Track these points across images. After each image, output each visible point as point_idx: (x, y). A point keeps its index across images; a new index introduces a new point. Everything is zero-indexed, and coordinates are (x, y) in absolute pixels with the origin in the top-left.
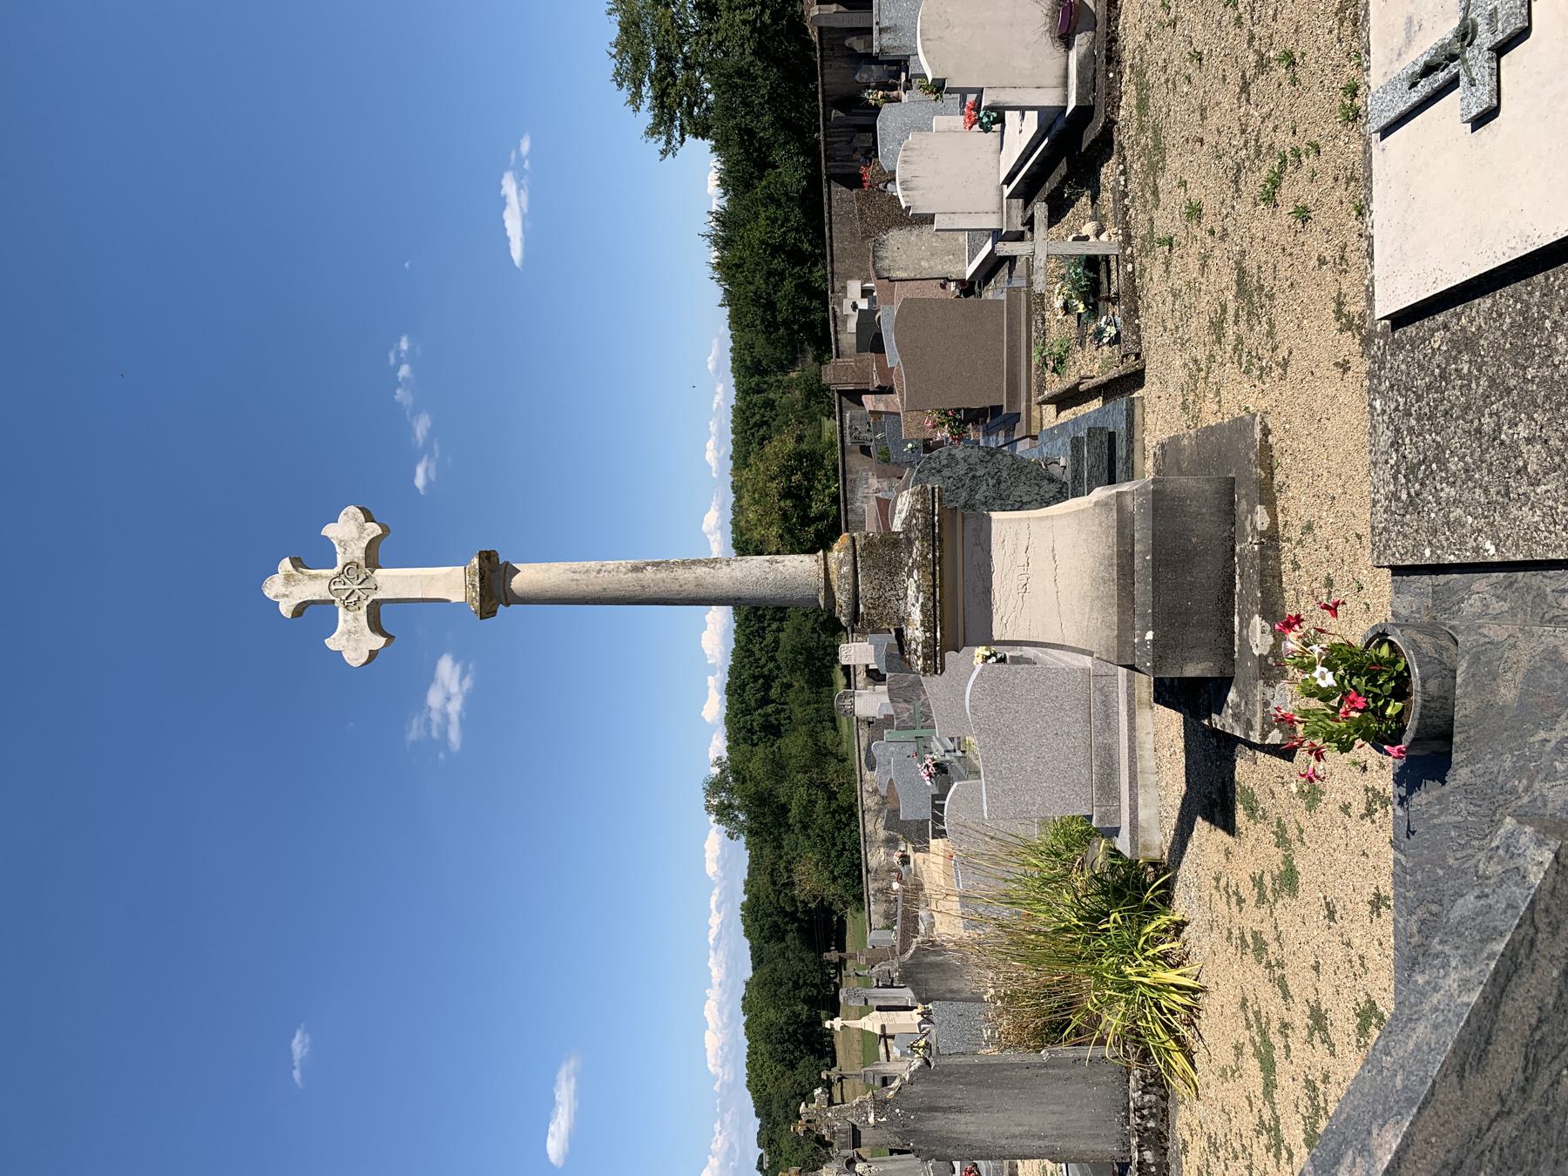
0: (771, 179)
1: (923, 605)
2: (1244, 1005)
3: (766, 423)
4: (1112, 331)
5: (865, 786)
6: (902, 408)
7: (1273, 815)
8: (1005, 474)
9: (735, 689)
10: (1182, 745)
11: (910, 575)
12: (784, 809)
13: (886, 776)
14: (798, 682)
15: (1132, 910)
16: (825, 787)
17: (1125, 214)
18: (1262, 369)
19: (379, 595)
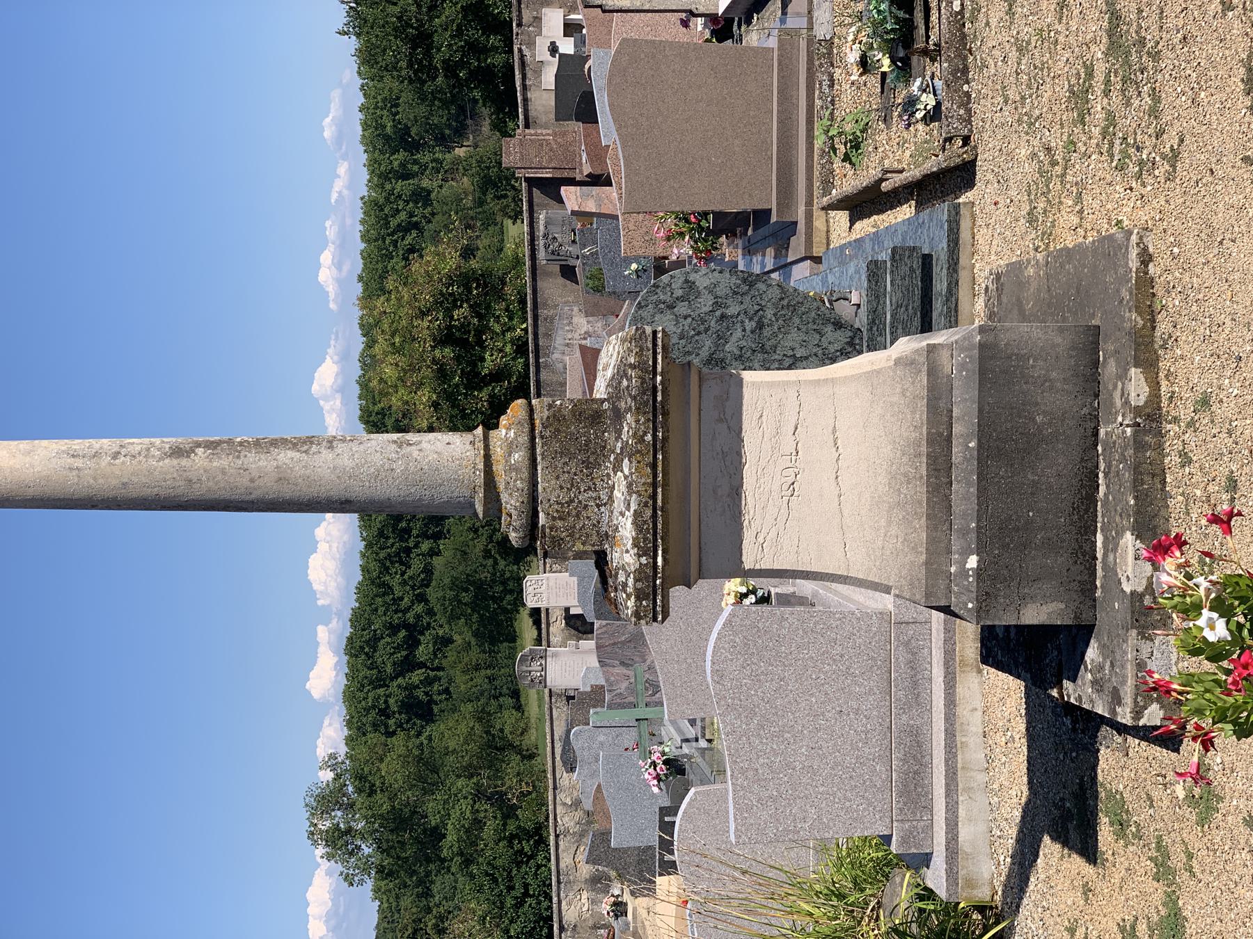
1: (637, 514)
3: (416, 226)
4: (928, 100)
5: (561, 796)
6: (628, 213)
7: (1150, 832)
8: (769, 313)
9: (361, 648)
10: (1022, 727)
11: (617, 467)
12: (437, 835)
13: (592, 782)
14: (462, 634)
16: (499, 799)
18: (1141, 163)
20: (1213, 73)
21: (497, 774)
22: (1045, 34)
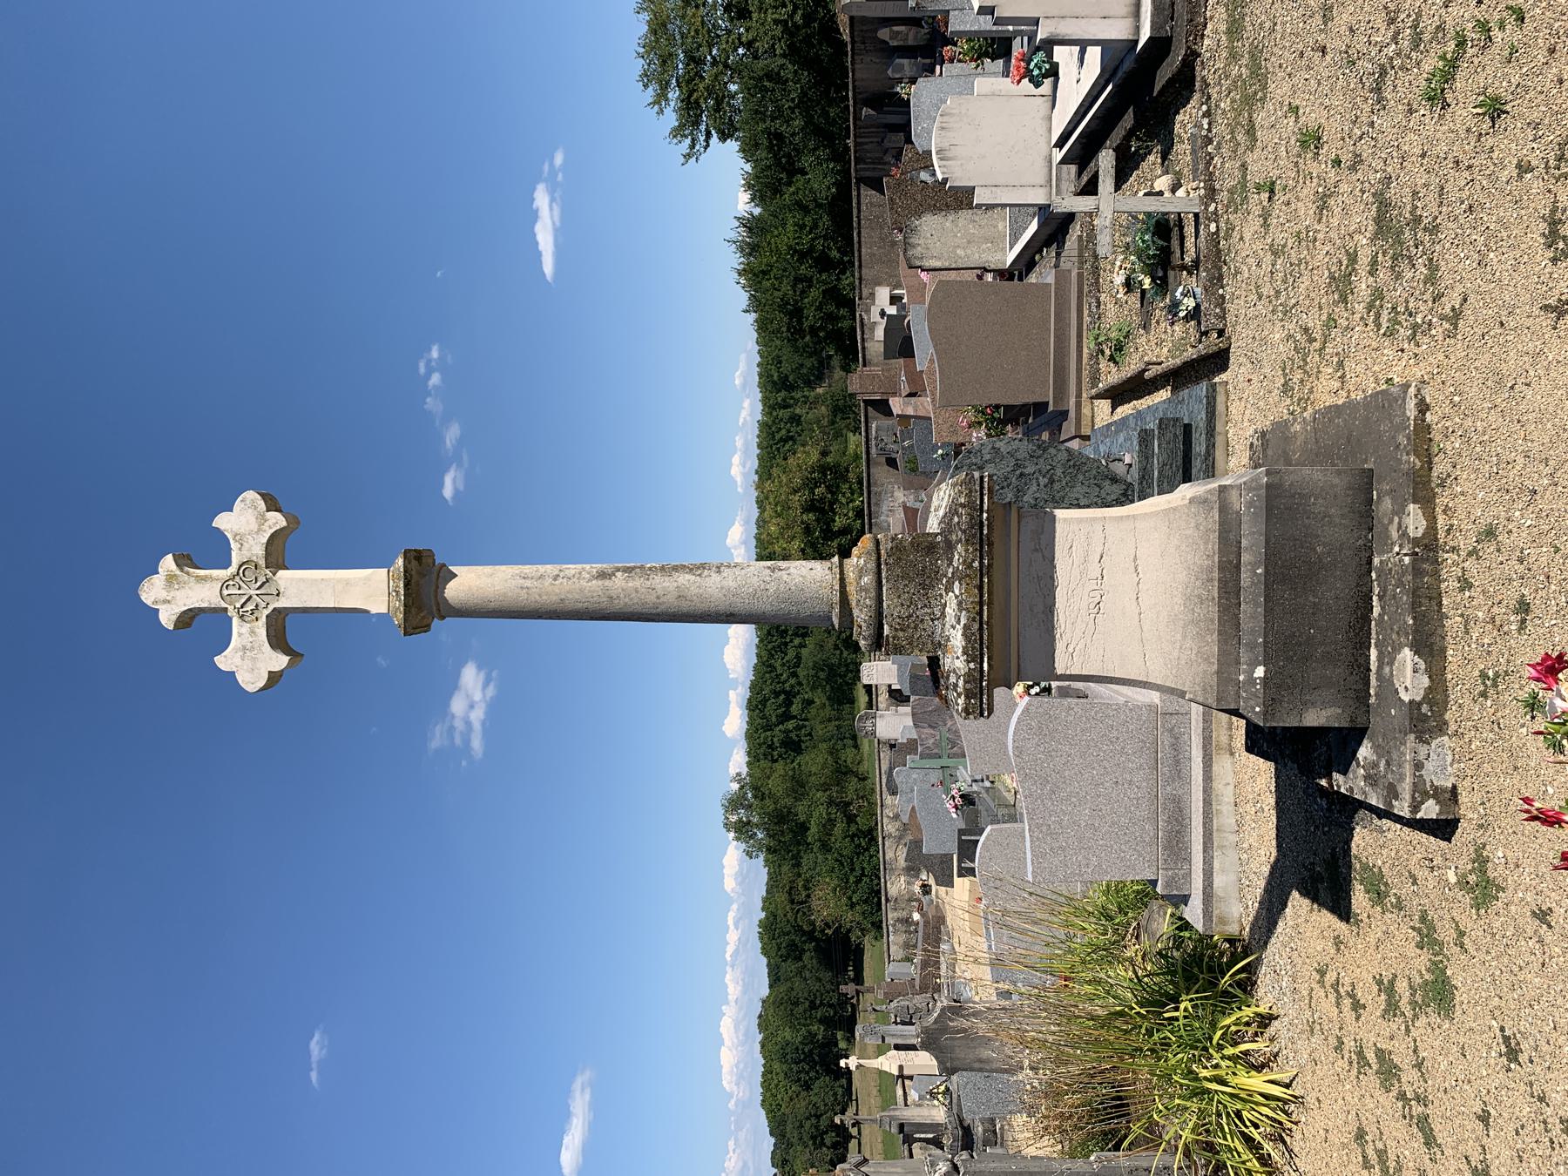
0: (800, 184)
1: (966, 627)
2: (1360, 1135)
3: (792, 438)
4: (1190, 303)
5: (886, 811)
7: (1414, 905)
8: (1059, 472)
9: (756, 705)
10: (1272, 801)
11: (949, 589)
12: (804, 828)
13: (910, 804)
14: (819, 698)
15: (1206, 998)
17: (1209, 163)
18: (1415, 327)
19: (282, 603)
20: (1504, 234)
21: (842, 790)
22: (1303, 236)
